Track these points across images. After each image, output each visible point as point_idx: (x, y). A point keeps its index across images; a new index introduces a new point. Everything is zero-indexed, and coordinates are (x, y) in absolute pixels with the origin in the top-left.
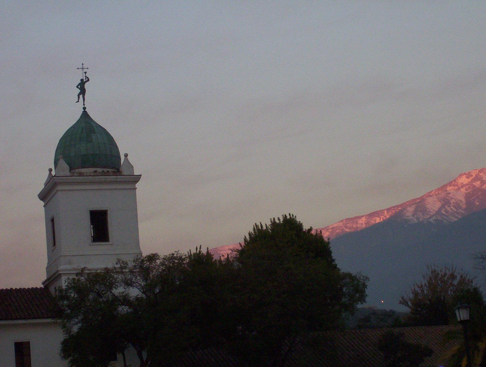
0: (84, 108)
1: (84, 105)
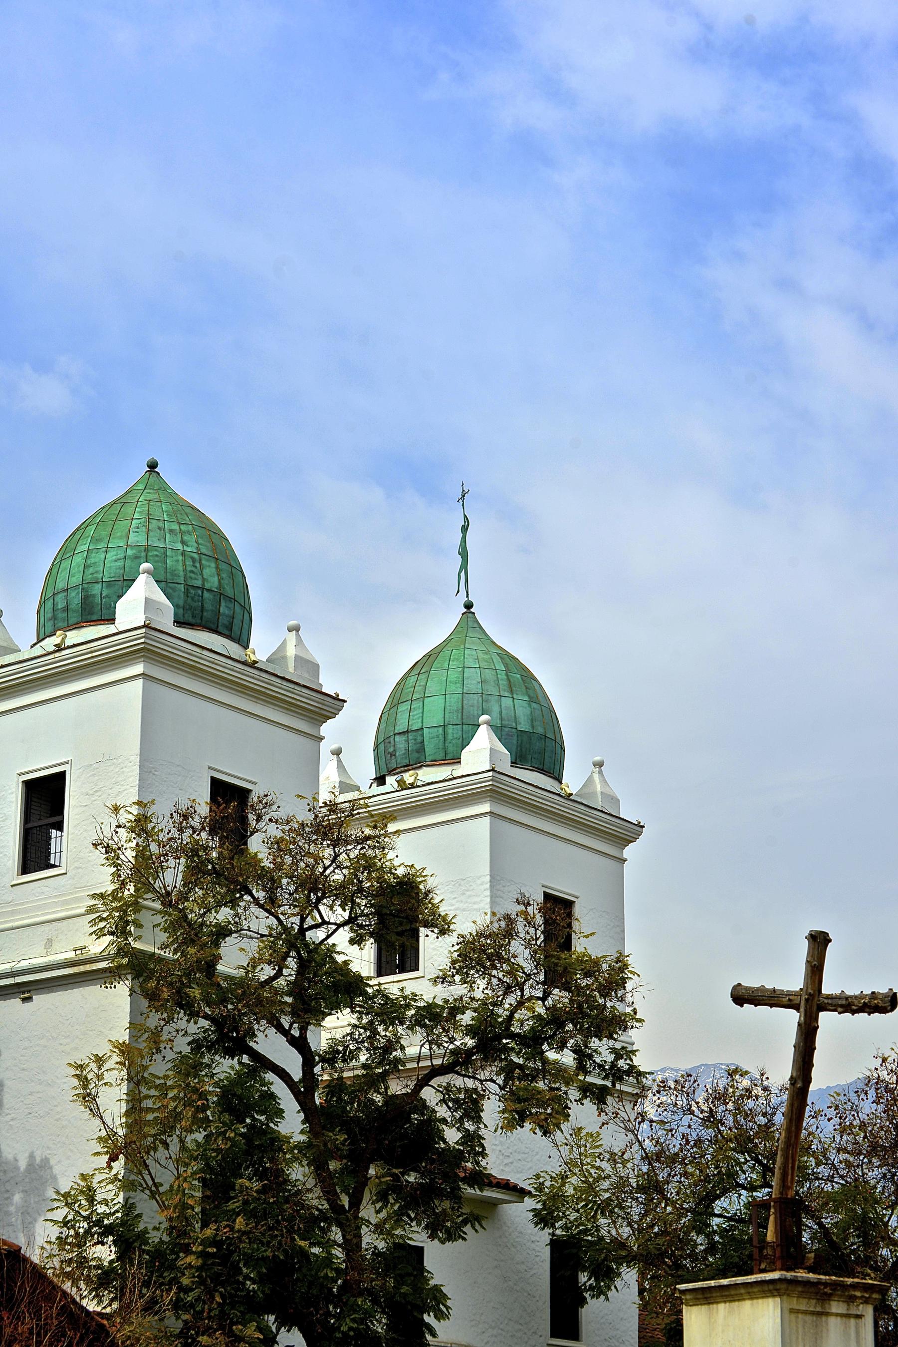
0: (469, 606)
1: (467, 596)
